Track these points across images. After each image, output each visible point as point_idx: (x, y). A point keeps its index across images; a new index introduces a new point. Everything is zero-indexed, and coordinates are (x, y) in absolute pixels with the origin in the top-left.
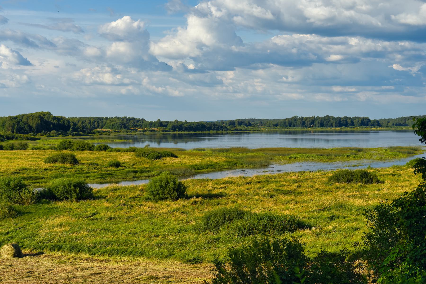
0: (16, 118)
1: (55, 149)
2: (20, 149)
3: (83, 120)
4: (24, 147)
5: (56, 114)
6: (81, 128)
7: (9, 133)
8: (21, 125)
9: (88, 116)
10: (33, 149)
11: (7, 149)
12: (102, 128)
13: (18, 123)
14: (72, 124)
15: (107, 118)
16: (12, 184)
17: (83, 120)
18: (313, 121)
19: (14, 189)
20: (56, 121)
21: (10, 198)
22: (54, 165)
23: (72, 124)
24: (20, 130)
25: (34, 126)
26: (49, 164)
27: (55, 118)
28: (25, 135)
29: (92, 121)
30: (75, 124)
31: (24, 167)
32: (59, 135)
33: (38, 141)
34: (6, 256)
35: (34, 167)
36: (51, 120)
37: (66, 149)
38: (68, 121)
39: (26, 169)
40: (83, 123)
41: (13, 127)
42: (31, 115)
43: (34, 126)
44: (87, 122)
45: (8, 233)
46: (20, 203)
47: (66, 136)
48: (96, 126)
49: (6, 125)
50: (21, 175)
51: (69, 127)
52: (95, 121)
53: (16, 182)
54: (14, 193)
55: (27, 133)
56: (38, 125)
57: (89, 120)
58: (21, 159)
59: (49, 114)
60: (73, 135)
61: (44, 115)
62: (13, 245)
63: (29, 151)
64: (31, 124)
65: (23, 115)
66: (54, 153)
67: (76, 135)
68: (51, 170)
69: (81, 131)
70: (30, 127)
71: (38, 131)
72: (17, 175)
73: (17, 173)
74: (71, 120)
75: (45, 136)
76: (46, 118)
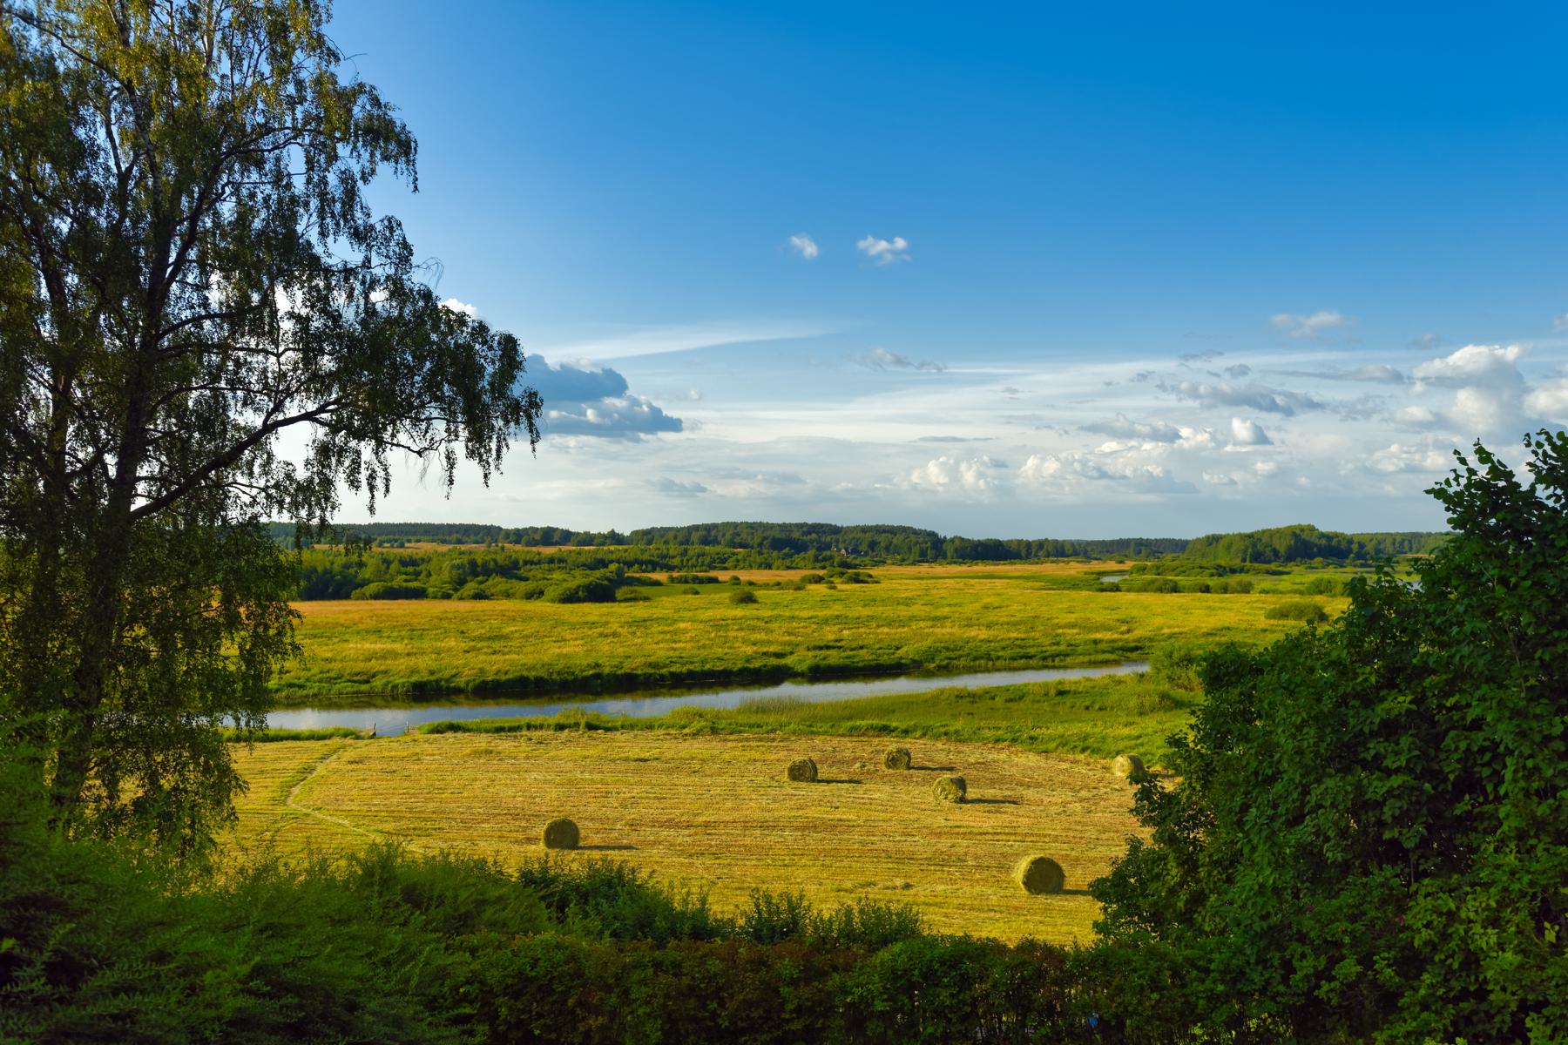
0: (1250, 536)
1: (1301, 593)
2: (1239, 592)
3: (1380, 537)
4: (1246, 589)
5: (1325, 526)
6: (1373, 553)
7: (1237, 562)
8: (1260, 547)
9: (1392, 531)
10: (1263, 592)
11: (1216, 592)
12: (1417, 552)
13: (1254, 545)
14: (1355, 547)
15: (1429, 534)
16: (1176, 656)
17: (1380, 539)
18: (711, 674)
19: (1178, 664)
20: (1323, 542)
21: (1170, 679)
22: (1281, 622)
23: (1355, 547)
24: (1257, 557)
25: (1282, 550)
26: (1272, 622)
27: (1323, 535)
28: (1264, 566)
29: (1399, 539)
30: (1362, 546)
31: (1227, 625)
32: (1328, 565)
33: (1285, 577)
34: (1119, 774)
35: (1243, 626)
36: (1314, 539)
37: (1321, 593)
38: (1350, 541)
39: (1229, 629)
40: (1379, 543)
41: (1245, 551)
42: (1278, 531)
43: (1282, 550)
44: (1389, 542)
45: (1139, 737)
46: (1186, 688)
47: (1342, 566)
48: (1407, 549)
49: (1234, 548)
50: (1217, 639)
51: (1350, 551)
52: (1404, 540)
53: (1182, 653)
54: (1178, 671)
55: (1269, 562)
56: (1289, 548)
57: (1393, 537)
58: (1230, 610)
59: (1312, 529)
60: (1355, 566)
61: (1302, 530)
62: (1131, 758)
63: (1254, 596)
64: (1278, 547)
65: (1264, 532)
66: (1297, 599)
67: (1362, 566)
68: (1273, 632)
69: (1372, 558)
70: (1275, 552)
71: (1290, 557)
72: (1211, 639)
73: (1211, 634)
74: (1356, 540)
75: (1302, 568)
76: (1305, 536)
